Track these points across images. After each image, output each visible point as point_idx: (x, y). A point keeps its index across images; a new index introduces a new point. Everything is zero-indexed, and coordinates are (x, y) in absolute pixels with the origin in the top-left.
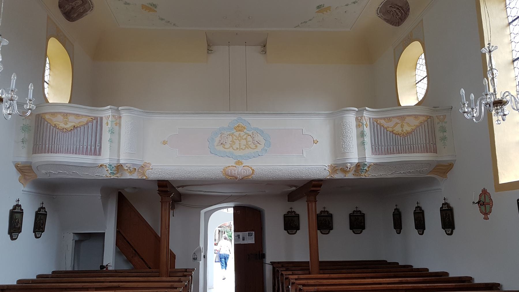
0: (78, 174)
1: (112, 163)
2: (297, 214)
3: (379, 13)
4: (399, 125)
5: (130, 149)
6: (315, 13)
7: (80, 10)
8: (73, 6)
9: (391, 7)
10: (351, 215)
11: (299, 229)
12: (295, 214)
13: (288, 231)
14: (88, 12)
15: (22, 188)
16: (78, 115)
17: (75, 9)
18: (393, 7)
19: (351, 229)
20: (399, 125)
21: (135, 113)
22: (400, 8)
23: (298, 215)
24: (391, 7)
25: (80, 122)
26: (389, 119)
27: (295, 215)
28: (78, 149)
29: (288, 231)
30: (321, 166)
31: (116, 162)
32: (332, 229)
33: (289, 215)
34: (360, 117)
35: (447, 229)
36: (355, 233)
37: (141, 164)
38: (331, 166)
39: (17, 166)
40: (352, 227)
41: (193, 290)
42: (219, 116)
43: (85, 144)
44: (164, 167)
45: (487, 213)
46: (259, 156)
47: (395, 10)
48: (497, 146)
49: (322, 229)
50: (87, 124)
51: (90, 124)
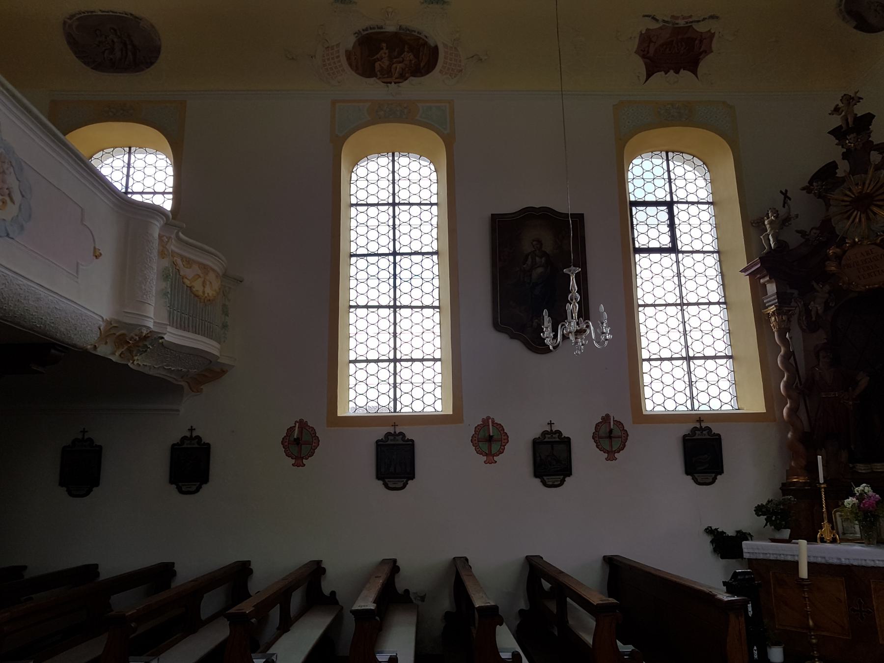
2: (408, 440)
3: (76, 19)
4: (200, 281)
6: (797, 232)
9: (115, 30)
12: (404, 441)
18: (119, 34)
20: (200, 281)
22: (129, 47)
23: (411, 443)
24: (115, 30)
26: (189, 262)
27: (401, 442)
29: (696, 475)
30: (96, 317)
33: (389, 442)
34: (167, 238)
35: (389, 480)
36: (700, 484)
38: (109, 323)
45: (302, 456)
46: (8, 235)
47: (115, 40)
48: (758, 411)
49: (545, 476)
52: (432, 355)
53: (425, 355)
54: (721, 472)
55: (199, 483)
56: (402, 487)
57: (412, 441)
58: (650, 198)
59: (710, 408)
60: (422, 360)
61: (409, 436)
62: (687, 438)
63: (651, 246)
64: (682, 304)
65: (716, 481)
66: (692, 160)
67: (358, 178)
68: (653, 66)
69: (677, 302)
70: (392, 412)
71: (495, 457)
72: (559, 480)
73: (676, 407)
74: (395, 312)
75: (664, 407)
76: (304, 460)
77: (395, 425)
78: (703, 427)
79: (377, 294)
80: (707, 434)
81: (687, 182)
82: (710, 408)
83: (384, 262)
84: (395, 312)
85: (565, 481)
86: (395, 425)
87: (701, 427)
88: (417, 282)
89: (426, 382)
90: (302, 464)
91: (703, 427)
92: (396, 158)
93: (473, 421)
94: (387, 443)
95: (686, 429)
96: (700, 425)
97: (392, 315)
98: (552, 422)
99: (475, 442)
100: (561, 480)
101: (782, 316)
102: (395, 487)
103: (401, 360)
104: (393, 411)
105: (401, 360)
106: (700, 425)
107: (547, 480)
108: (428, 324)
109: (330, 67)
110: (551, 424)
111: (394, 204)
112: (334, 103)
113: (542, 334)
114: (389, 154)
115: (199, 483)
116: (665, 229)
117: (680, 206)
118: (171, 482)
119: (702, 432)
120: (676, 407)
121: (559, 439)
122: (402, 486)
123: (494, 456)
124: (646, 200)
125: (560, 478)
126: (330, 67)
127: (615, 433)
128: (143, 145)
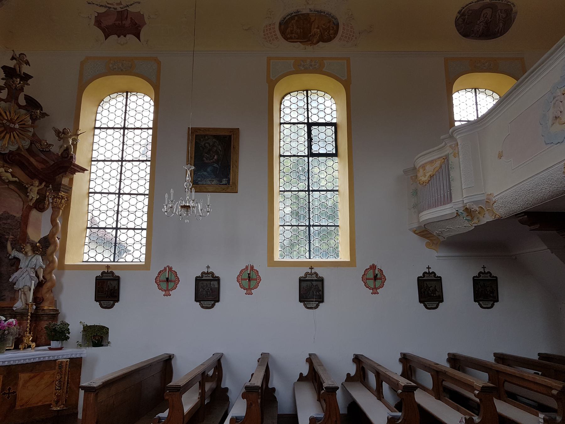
0: (452, 229)
1: (457, 208)
2: (438, 277)
5: (465, 183)
7: (499, 16)
8: (485, 21)
10: (98, 279)
11: (497, 301)
13: (481, 302)
14: (514, 9)
15: (434, 253)
16: (432, 162)
17: (491, 21)
19: (421, 301)
21: (464, 131)
25: (434, 169)
28: (437, 200)
31: (461, 205)
32: (498, 301)
37: (484, 198)
39: (414, 232)
40: (302, 299)
41: (467, 411)
42: (545, 67)
43: (442, 193)
44: (503, 194)
50: (441, 167)
51: (443, 166)
52: (141, 226)
53: (121, 225)
54: (118, 301)
55: (492, 302)
56: (436, 307)
57: (440, 277)
58: (322, 121)
59: (96, 260)
60: (134, 229)
61: (320, 275)
62: (475, 278)
63: (320, 152)
64: (309, 190)
65: (439, 306)
66: (484, 92)
67: (312, 107)
68: (108, 32)
69: (116, 192)
70: (307, 259)
71: (377, 290)
72: (211, 304)
73: (103, 259)
74: (119, 197)
75: (95, 259)
76: (170, 291)
77: (311, 268)
78: (486, 272)
79: (108, 185)
80: (204, 277)
81: (319, 111)
82: (96, 260)
83: (115, 165)
84: (119, 197)
85: (115, 305)
86: (311, 268)
87: (429, 272)
88: (135, 177)
89: (121, 243)
90: (169, 294)
91: (486, 272)
92: (129, 97)
93: (363, 265)
94: (203, 278)
95: (99, 273)
96: (429, 270)
97: (117, 199)
98: (428, 267)
99: (364, 280)
100: (212, 304)
101: (57, 199)
102: (487, 307)
103: (120, 228)
104: (308, 258)
105: (120, 228)
106: (429, 270)
107: (103, 304)
108: (140, 206)
109: (268, 36)
110: (429, 268)
111: (124, 128)
112: (269, 59)
113: (163, 210)
114: (124, 93)
115: (492, 302)
116: (315, 139)
117: (120, 126)
118: (475, 301)
119: (429, 275)
120: (103, 259)
121: (212, 277)
122: (436, 306)
123: (169, 290)
124: (333, 122)
125: (212, 303)
126: (268, 36)
127: (379, 276)
128: (137, 91)
